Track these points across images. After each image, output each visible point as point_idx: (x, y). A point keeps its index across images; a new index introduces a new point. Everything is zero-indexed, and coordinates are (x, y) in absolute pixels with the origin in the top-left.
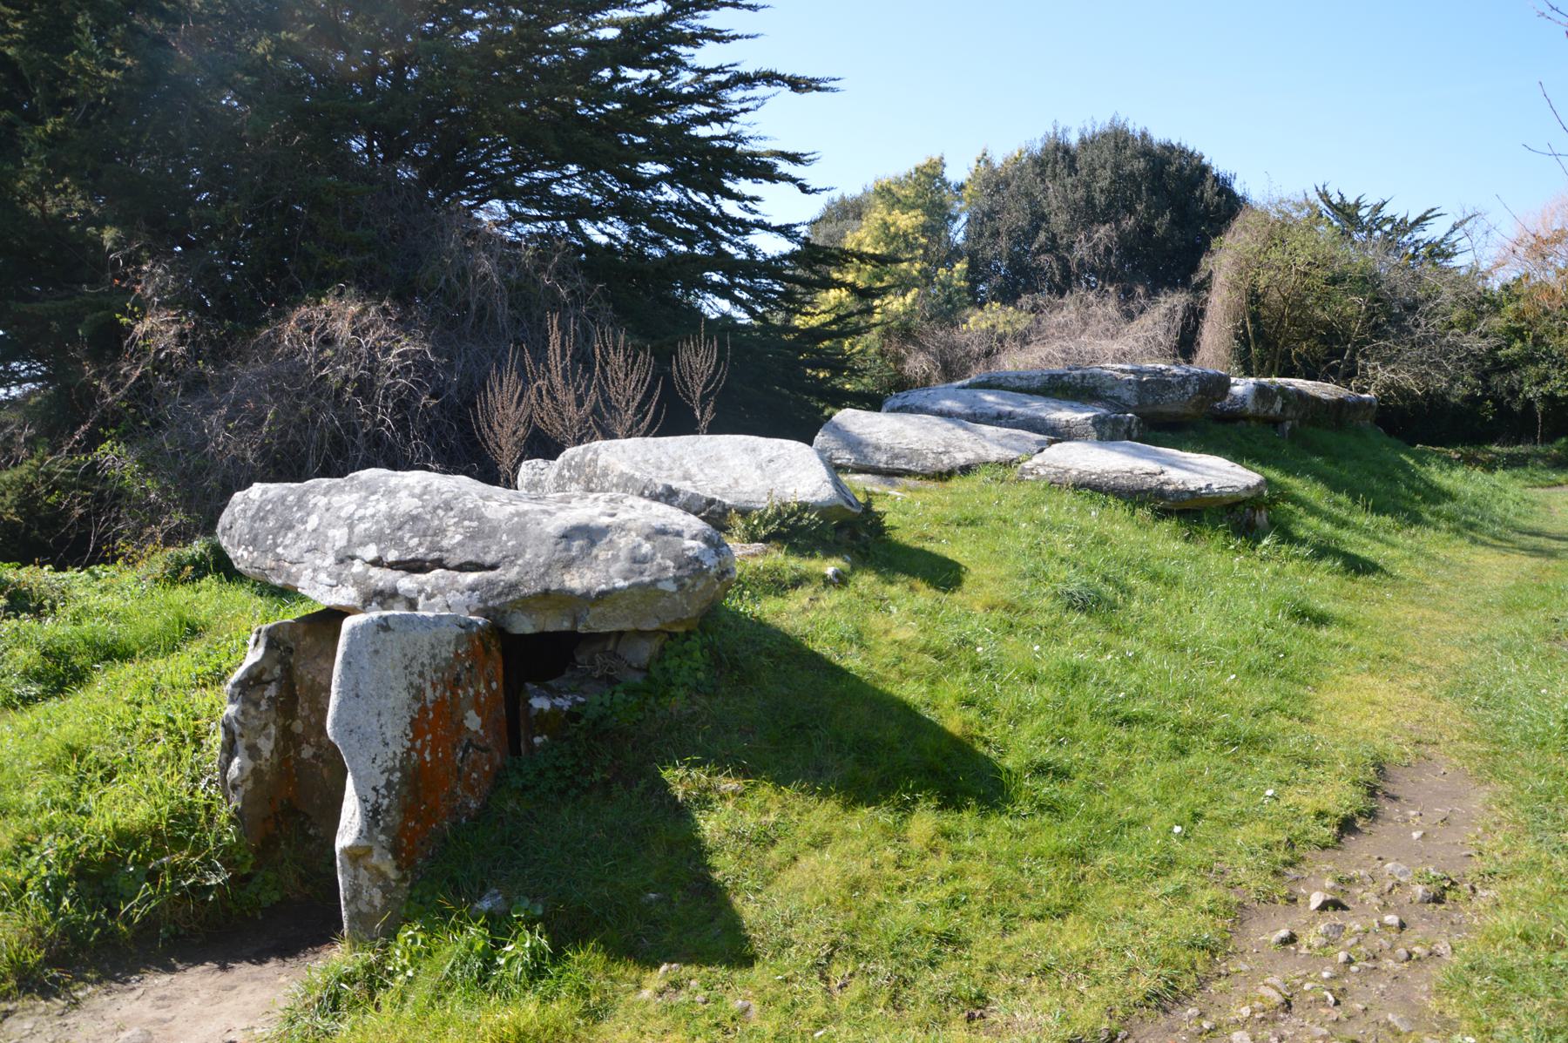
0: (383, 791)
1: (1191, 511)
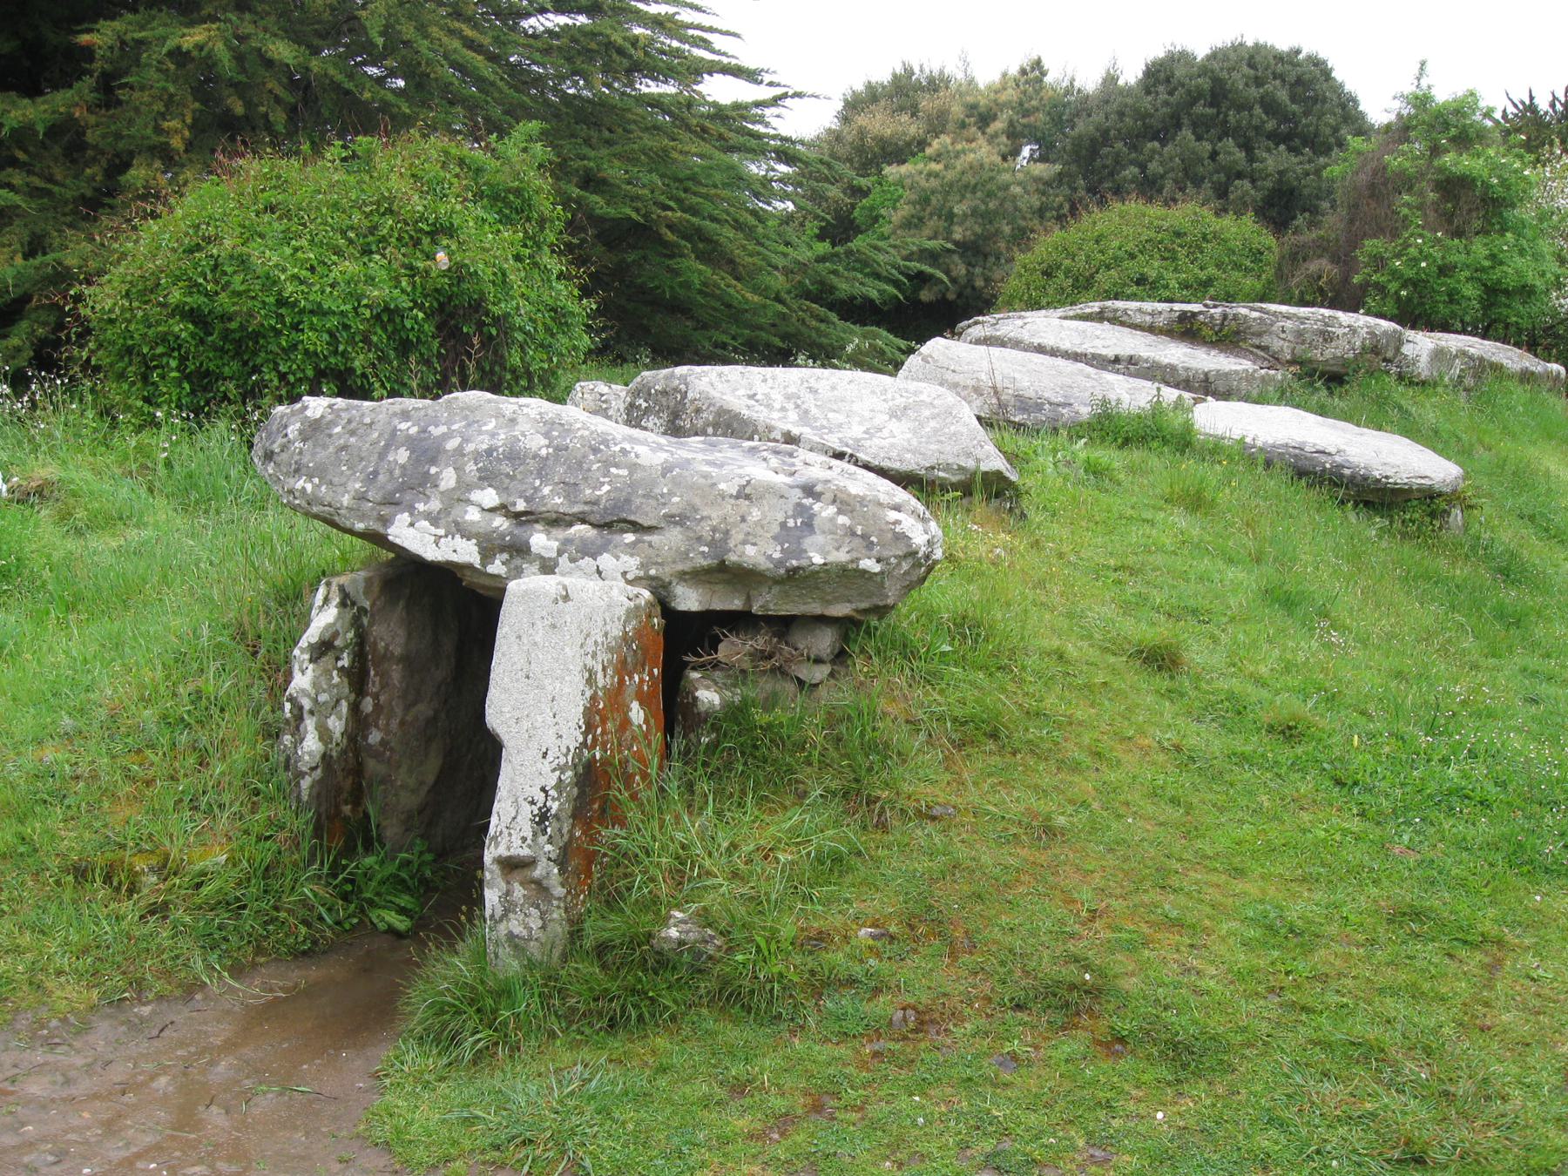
0: (553, 793)
1: (1375, 497)
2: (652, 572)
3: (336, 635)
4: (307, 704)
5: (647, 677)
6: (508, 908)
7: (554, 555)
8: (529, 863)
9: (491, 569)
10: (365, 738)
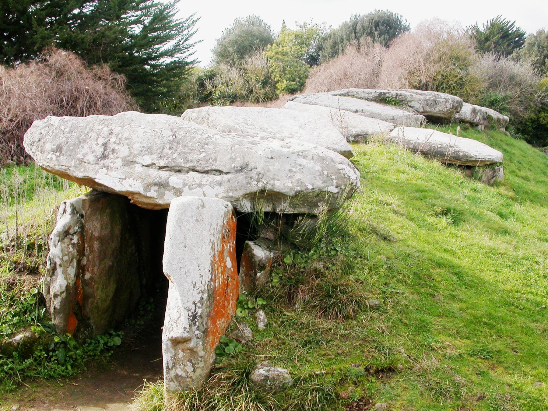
0: (199, 305)
1: (468, 166)
2: (231, 194)
3: (69, 228)
4: (58, 262)
5: (231, 245)
6: (175, 362)
7: (182, 186)
8: (186, 340)
9: (149, 194)
10: (83, 276)
